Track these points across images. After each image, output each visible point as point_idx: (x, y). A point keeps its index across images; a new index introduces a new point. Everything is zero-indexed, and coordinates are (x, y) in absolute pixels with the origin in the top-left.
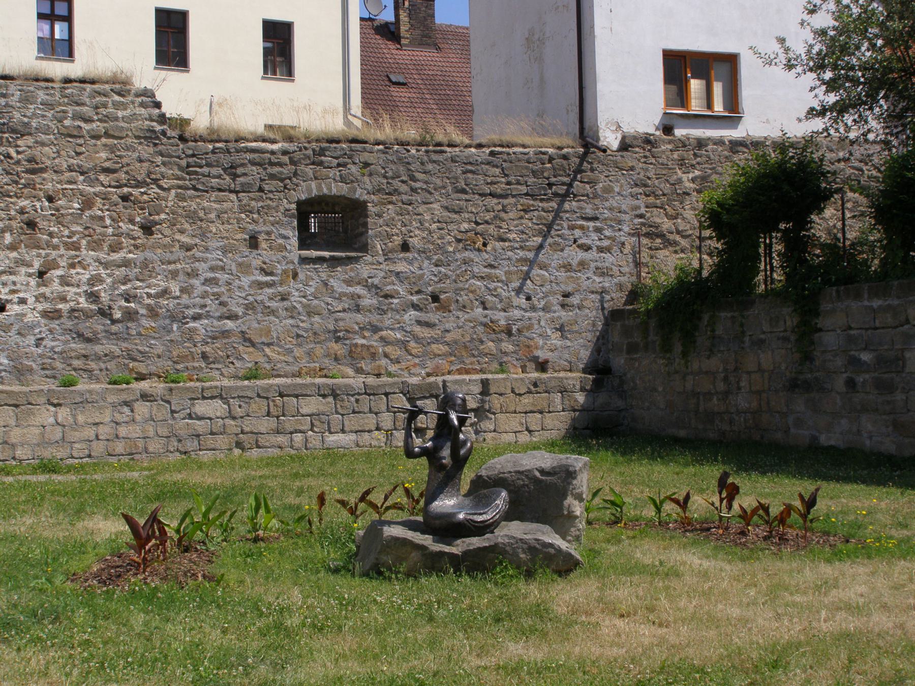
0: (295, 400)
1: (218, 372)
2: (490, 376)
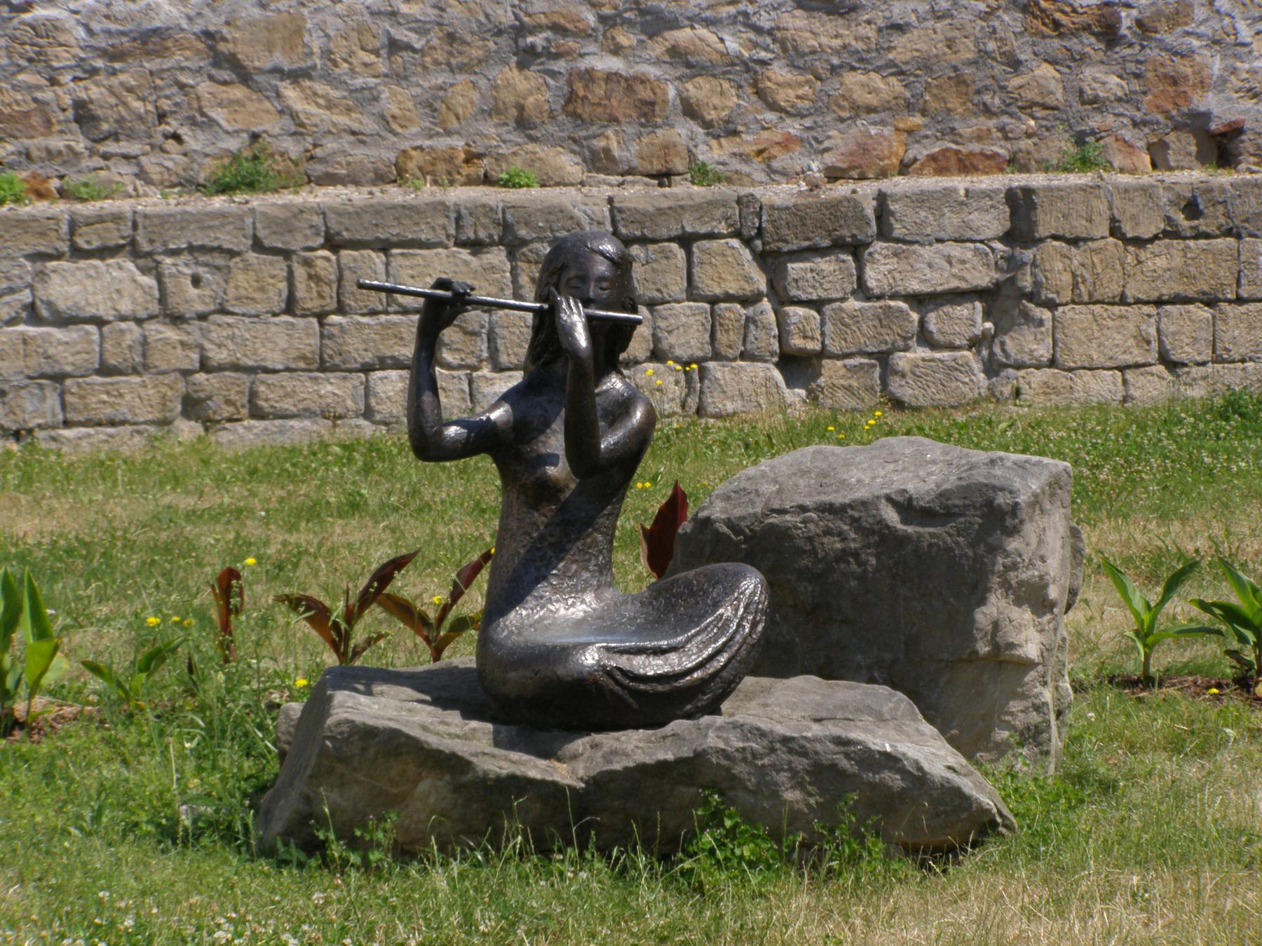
0: (378, 259)
1: (128, 169)
2: (1037, 180)
